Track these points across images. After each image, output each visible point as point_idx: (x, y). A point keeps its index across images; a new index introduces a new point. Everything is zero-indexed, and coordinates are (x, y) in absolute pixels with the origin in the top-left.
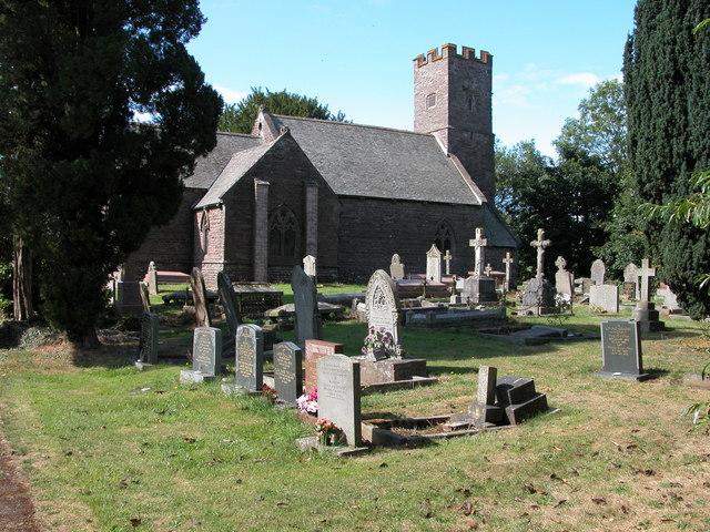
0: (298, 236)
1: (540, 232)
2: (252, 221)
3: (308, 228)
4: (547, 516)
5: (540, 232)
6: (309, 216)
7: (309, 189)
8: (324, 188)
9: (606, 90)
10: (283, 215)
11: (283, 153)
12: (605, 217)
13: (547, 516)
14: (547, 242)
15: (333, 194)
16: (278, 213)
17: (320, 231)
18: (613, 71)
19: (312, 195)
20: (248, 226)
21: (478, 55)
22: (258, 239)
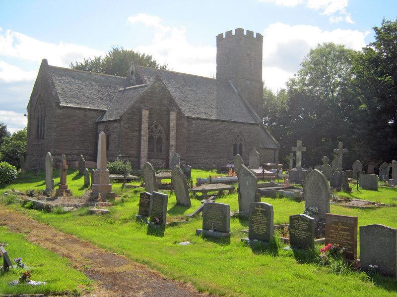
0: (164, 140)
1: (299, 143)
2: (140, 130)
3: (171, 136)
4: (137, 295)
5: (299, 143)
6: (171, 129)
7: (171, 113)
8: (180, 115)
9: (342, 55)
10: (156, 127)
11: (156, 90)
12: (54, 159)
13: (137, 295)
14: (304, 149)
15: (184, 116)
16: (153, 126)
17: (177, 139)
18: (359, 40)
19: (173, 116)
20: (137, 134)
21: (255, 36)
22: (142, 142)
